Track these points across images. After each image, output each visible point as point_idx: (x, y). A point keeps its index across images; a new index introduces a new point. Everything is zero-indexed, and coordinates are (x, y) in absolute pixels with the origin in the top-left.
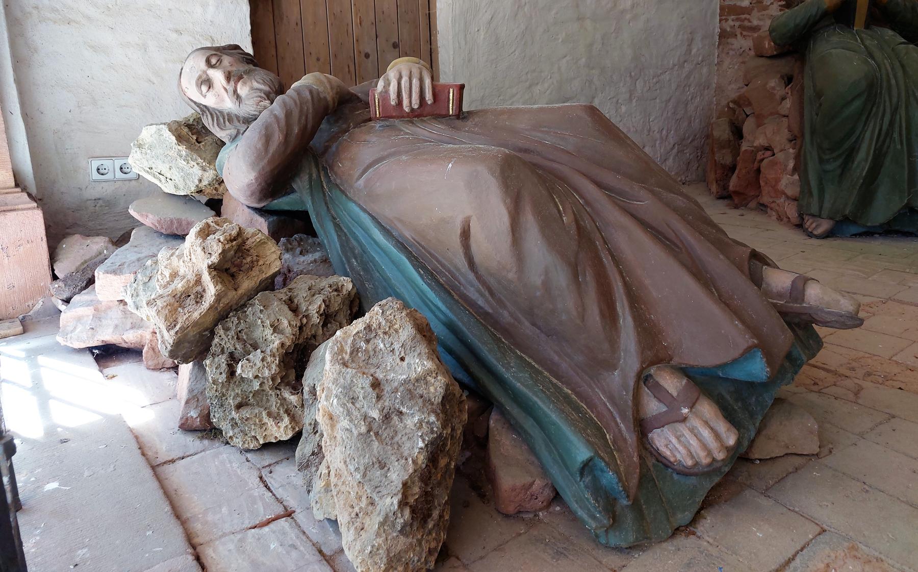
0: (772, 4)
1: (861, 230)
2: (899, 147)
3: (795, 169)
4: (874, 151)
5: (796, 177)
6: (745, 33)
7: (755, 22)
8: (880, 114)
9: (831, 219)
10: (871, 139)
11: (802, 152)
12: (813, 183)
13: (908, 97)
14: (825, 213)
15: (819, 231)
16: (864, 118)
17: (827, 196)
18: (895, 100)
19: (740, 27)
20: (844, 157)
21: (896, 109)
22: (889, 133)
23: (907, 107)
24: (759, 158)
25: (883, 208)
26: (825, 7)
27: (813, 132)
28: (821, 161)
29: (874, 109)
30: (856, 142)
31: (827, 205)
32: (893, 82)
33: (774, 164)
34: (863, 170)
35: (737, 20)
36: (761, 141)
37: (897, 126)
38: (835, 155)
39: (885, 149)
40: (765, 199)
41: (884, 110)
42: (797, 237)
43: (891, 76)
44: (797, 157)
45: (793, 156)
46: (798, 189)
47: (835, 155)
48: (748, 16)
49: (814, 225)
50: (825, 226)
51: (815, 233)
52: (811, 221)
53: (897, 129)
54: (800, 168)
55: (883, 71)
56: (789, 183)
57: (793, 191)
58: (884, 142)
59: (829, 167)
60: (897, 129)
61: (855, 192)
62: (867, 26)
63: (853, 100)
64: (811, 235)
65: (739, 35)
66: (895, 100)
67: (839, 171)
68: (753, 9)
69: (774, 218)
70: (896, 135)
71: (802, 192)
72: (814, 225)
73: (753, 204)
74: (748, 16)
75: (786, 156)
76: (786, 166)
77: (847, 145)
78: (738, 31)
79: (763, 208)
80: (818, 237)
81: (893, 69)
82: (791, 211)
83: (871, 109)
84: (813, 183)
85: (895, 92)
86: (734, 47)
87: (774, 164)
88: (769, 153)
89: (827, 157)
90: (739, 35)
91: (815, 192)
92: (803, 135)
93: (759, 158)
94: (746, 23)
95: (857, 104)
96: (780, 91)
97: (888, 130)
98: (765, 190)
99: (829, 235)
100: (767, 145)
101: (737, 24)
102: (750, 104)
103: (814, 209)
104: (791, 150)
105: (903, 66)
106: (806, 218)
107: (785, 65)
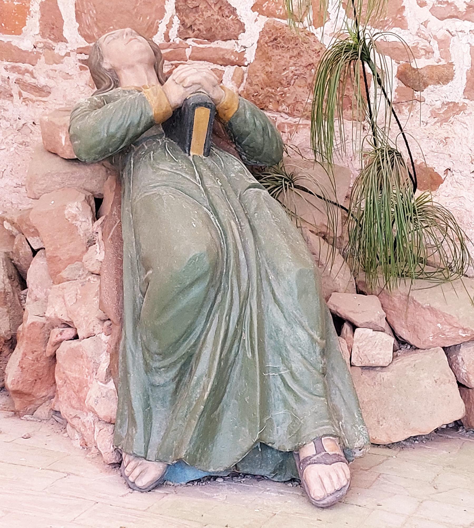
0: (68, 54)
1: (201, 475)
2: (249, 355)
3: (110, 373)
4: (219, 363)
5: (111, 385)
6: (25, 94)
7: (42, 81)
8: (227, 307)
9: (159, 460)
10: (215, 344)
11: (121, 348)
12: (137, 405)
13: (260, 286)
14: (152, 452)
15: (143, 482)
16: (206, 311)
17: (156, 425)
18: (244, 286)
19: (18, 82)
20: (179, 366)
21: (246, 298)
22: (238, 334)
23: (259, 296)
24: (54, 338)
25: (229, 448)
26: (152, 114)
27: (137, 320)
28: (148, 370)
29: (219, 298)
30: (195, 345)
31: (155, 439)
32: (242, 257)
33: (76, 355)
34: (204, 390)
35: (14, 69)
36: (56, 310)
37: (247, 322)
38: (167, 362)
39: (232, 358)
40: (64, 408)
41: (232, 300)
42: (109, 483)
43: (240, 248)
44: (114, 355)
45: (105, 346)
46: (115, 406)
47: (167, 362)
48: (30, 67)
49: (137, 471)
50: (153, 471)
51: (139, 484)
52: (132, 464)
53: (247, 329)
54: (117, 371)
55: (230, 241)
56: (101, 395)
57: (108, 408)
58: (230, 350)
59: (158, 379)
60: (247, 329)
61: (194, 423)
62: (208, 153)
63: (192, 285)
64: (132, 486)
65: (16, 97)
66: (244, 286)
67: (173, 386)
68: (38, 56)
69: (77, 443)
70: (246, 336)
71: (119, 413)
72: (137, 471)
73: (43, 411)
74: (30, 67)
75: (96, 349)
76: (97, 365)
77: (184, 349)
78: (15, 89)
79: (58, 419)
80: (141, 490)
81: (241, 233)
82: (104, 441)
83: (216, 297)
84: (137, 405)
85: (244, 275)
86: (8, 115)
87: (76, 355)
88: (69, 333)
89: (157, 364)
90: (16, 97)
91: (139, 417)
92: (122, 321)
93: (54, 338)
94: (27, 78)
95: (197, 290)
96: (85, 224)
97: (236, 330)
98: (64, 393)
99: (159, 484)
100: (66, 319)
101: (14, 76)
102: (36, 233)
103: (138, 447)
104: (104, 337)
105: (253, 229)
106: (126, 459)
107: (93, 178)
